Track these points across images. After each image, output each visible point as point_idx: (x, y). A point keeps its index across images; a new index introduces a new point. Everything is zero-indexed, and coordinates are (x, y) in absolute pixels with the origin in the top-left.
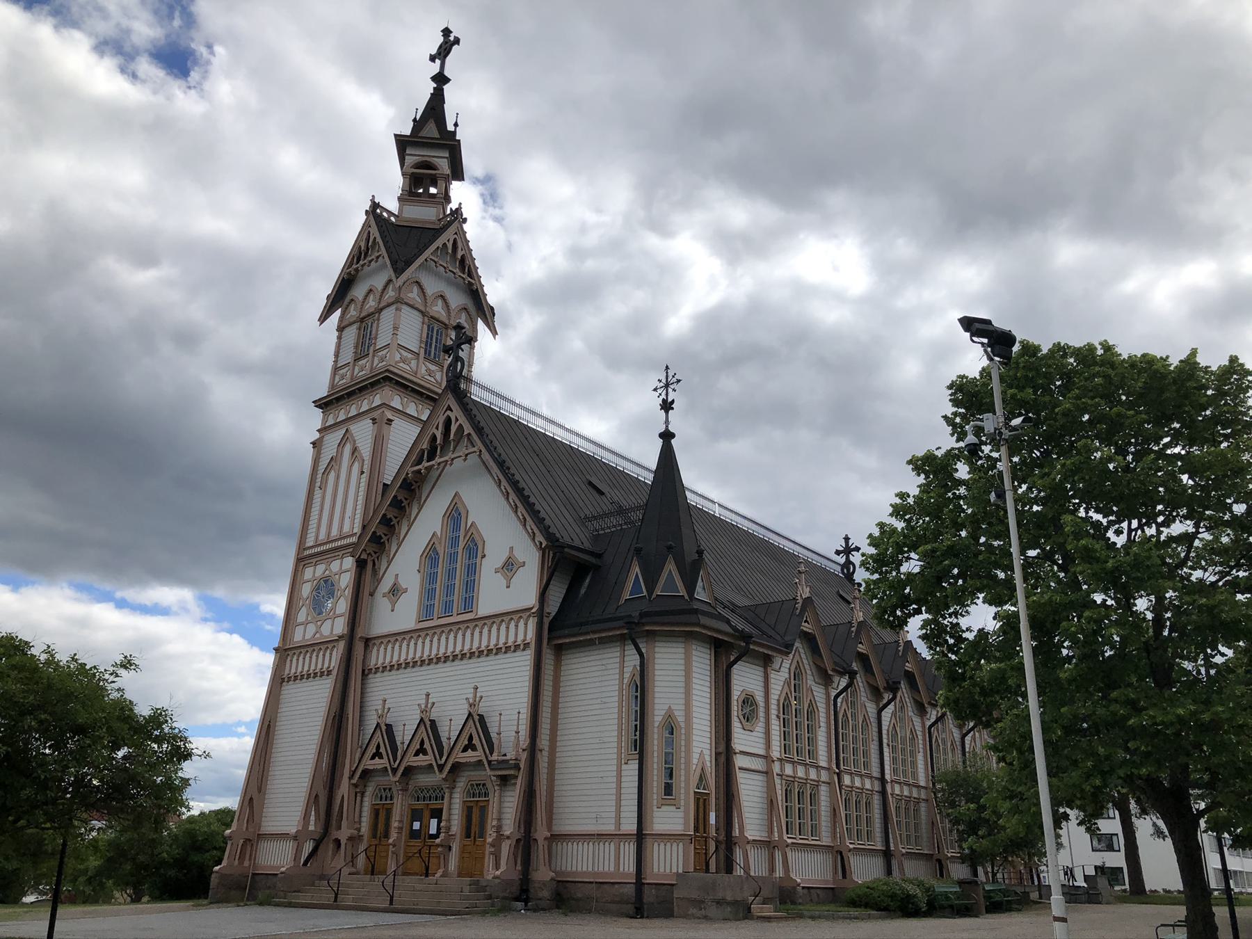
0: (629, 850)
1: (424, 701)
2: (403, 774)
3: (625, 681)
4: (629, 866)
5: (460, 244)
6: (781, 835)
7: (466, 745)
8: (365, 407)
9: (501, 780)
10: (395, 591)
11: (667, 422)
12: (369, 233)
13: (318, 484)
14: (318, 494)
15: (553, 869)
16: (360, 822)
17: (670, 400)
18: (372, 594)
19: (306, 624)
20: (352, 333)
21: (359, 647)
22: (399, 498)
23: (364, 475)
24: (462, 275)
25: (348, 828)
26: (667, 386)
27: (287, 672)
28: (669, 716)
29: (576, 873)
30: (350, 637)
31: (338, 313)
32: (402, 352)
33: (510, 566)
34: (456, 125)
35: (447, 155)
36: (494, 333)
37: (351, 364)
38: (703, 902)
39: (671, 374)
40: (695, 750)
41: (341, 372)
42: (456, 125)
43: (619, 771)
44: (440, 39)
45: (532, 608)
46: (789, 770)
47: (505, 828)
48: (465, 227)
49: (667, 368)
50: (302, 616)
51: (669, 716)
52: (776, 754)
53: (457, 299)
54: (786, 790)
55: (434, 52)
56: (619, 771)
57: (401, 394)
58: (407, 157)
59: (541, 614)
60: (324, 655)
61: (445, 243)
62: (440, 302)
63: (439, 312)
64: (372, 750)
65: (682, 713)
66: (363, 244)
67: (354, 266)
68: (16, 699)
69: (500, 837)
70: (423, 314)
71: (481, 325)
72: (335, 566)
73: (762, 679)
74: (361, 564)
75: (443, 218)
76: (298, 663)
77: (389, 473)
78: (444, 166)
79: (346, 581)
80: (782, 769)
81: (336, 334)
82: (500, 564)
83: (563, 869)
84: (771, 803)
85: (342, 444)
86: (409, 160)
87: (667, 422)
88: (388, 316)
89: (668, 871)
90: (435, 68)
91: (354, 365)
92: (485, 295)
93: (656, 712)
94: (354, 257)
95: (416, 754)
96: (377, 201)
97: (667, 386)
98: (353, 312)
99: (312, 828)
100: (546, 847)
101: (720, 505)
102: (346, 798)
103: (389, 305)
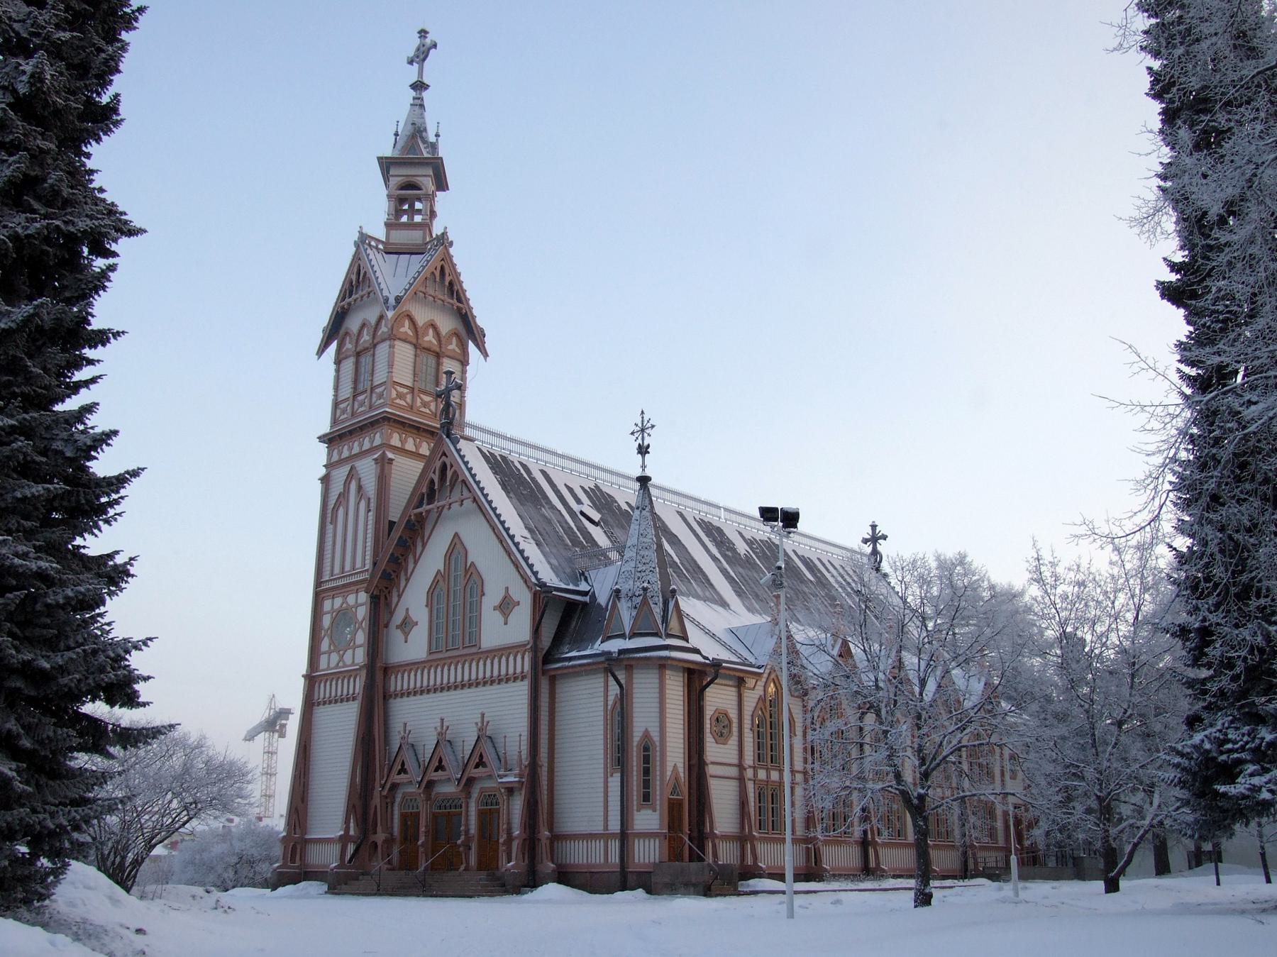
0: (615, 846)
1: (439, 724)
3: (609, 707)
4: (614, 858)
5: (447, 271)
6: (750, 830)
7: (477, 763)
8: (367, 446)
9: (508, 791)
10: (407, 625)
11: (644, 467)
12: (359, 266)
13: (329, 519)
14: (330, 528)
15: (556, 861)
16: (392, 828)
17: (646, 444)
18: (387, 626)
19: (329, 652)
20: (349, 365)
21: (379, 676)
23: (370, 514)
24: (451, 301)
25: (383, 832)
26: (643, 430)
27: (316, 697)
28: (646, 735)
29: (578, 866)
31: (334, 346)
32: (398, 388)
33: (506, 606)
34: (437, 135)
35: (432, 174)
36: (485, 355)
38: (674, 885)
39: (646, 419)
40: (668, 764)
41: (342, 406)
42: (437, 135)
43: (606, 782)
45: (525, 645)
46: (762, 774)
47: (514, 830)
48: (452, 251)
49: (643, 412)
50: (325, 645)
51: (646, 735)
52: (749, 759)
53: (447, 324)
54: (759, 794)
55: (411, 54)
56: (606, 782)
58: (390, 179)
59: (535, 649)
62: (431, 331)
63: (430, 341)
64: (398, 767)
65: (657, 734)
66: (354, 277)
67: (347, 300)
68: (54, 720)
69: (468, 839)
70: (416, 346)
71: (472, 347)
72: (351, 599)
73: (735, 698)
75: (430, 242)
77: (395, 514)
78: (429, 184)
79: (362, 613)
80: (755, 774)
81: (333, 367)
82: (497, 603)
83: (568, 862)
84: (743, 803)
85: (347, 483)
86: (394, 181)
87: (644, 467)
88: (383, 350)
89: (647, 861)
90: (412, 74)
91: (354, 400)
92: (474, 317)
93: (635, 734)
94: (345, 292)
95: (436, 770)
96: (364, 231)
97: (643, 430)
98: (349, 346)
99: (352, 832)
100: (548, 845)
101: (726, 509)
103: (383, 341)
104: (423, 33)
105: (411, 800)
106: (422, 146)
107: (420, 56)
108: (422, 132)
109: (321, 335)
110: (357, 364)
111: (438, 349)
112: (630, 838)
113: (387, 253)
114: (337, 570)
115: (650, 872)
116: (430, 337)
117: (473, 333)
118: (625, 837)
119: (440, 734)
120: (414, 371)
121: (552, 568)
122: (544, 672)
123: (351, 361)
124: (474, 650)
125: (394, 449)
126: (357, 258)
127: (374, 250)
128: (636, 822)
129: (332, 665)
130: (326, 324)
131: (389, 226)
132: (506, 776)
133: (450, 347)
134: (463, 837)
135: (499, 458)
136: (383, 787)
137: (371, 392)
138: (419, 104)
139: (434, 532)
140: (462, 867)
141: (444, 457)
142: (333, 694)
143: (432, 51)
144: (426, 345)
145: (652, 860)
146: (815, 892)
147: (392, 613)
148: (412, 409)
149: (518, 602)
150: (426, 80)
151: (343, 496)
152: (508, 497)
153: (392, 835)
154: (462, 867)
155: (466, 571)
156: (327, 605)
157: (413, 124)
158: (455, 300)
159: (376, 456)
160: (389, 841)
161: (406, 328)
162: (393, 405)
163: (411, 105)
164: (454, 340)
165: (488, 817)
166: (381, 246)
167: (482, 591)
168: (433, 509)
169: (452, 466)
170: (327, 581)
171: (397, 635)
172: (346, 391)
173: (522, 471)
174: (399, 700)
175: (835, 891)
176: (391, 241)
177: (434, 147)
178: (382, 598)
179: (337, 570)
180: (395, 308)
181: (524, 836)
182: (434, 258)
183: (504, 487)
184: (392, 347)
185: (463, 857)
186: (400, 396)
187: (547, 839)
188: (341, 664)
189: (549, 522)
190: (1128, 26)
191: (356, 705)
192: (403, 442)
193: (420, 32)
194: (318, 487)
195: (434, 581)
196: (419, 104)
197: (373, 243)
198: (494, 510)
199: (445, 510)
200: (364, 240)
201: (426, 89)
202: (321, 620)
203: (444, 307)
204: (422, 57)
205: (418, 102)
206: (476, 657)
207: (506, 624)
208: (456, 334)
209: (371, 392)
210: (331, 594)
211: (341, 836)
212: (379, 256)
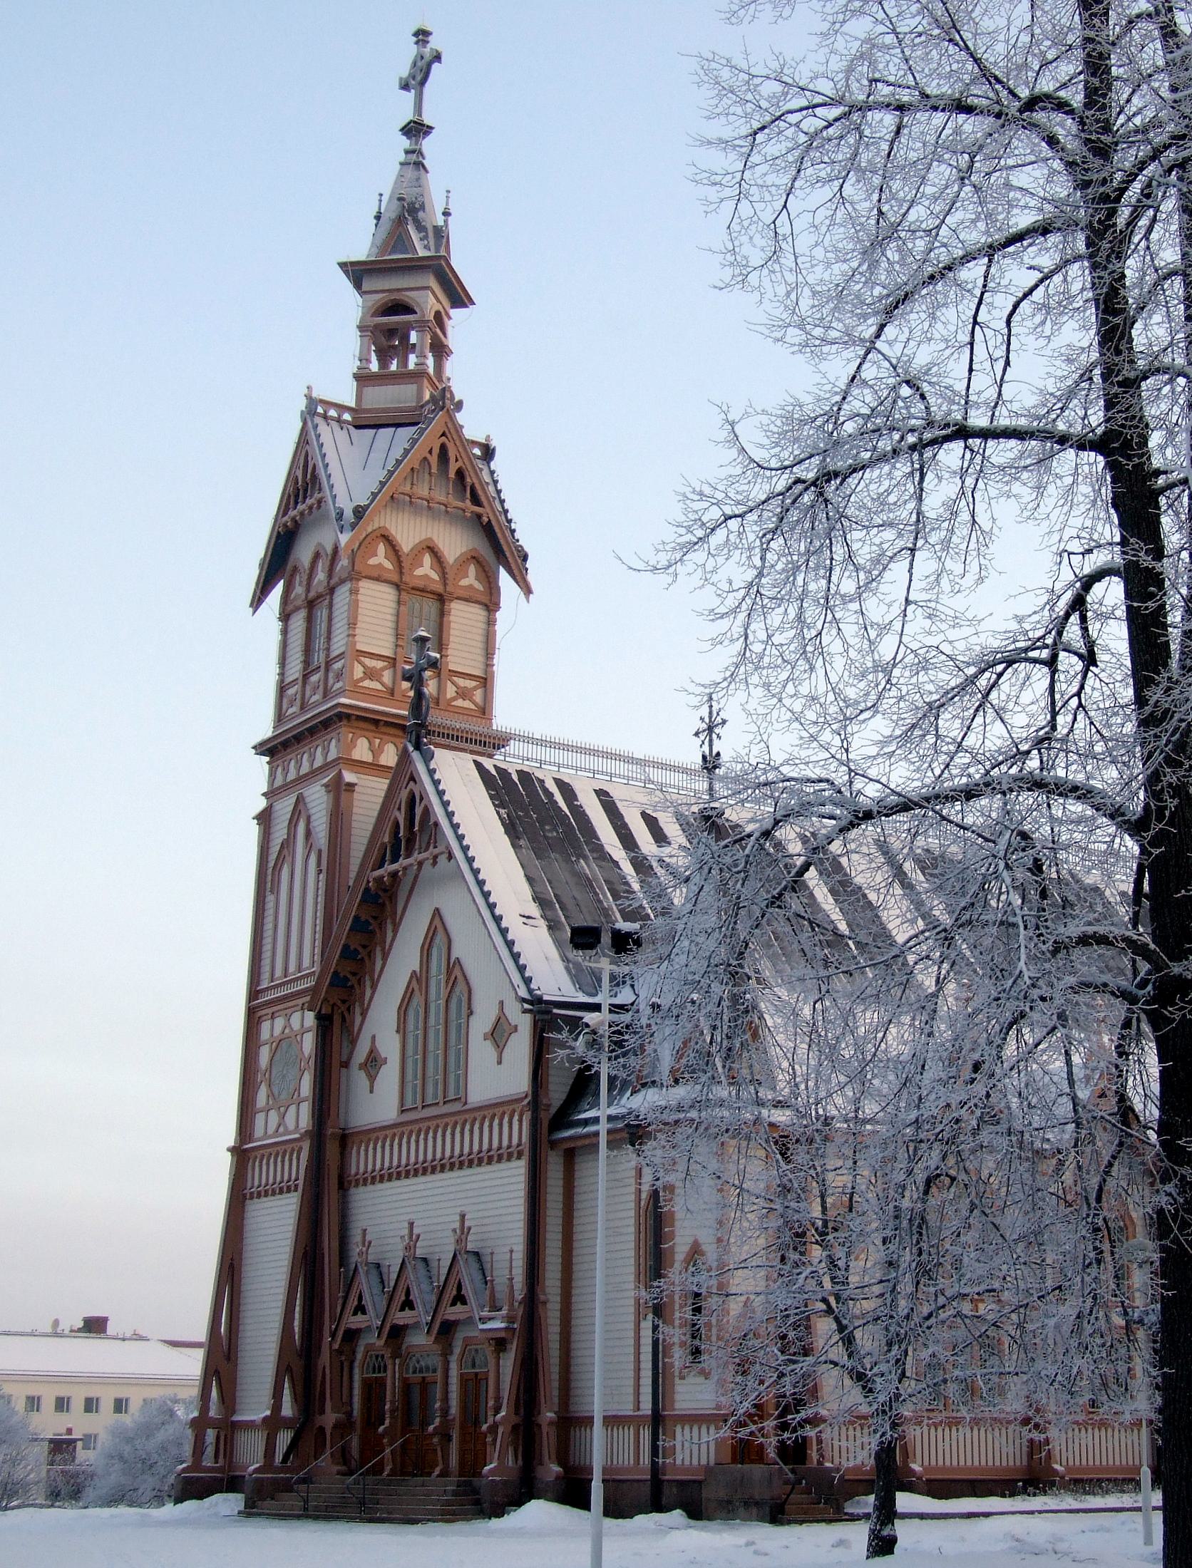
2: (389, 1336)
5: (452, 454)
10: (373, 1063)
14: (270, 899)
16: (351, 1404)
18: (346, 1064)
20: (298, 622)
21: (332, 1150)
22: (363, 919)
24: (460, 504)
30: (318, 1134)
31: (278, 590)
34: (446, 214)
36: (528, 590)
37: (300, 682)
42: (446, 214)
44: (408, 51)
45: (522, 1099)
48: (461, 417)
50: (262, 1098)
55: (405, 73)
57: (367, 734)
60: (491, 1127)
61: (425, 459)
62: (427, 559)
66: (300, 474)
67: (292, 513)
70: (397, 586)
71: (504, 578)
74: (325, 1024)
76: (392, 1149)
79: (309, 1043)
81: (277, 626)
82: (488, 1027)
85: (293, 823)
88: (342, 595)
89: (695, 1462)
90: (404, 108)
96: (314, 395)
102: (328, 1371)
103: (342, 582)
104: (422, 35)
105: (377, 1357)
106: (414, 236)
107: (417, 79)
108: (418, 210)
109: (257, 572)
110: (310, 620)
111: (439, 588)
112: (669, 1423)
113: (358, 427)
114: (278, 973)
115: (700, 1482)
116: (426, 569)
117: (505, 555)
118: (658, 1421)
119: (407, 1248)
120: (397, 629)
121: (567, 969)
122: (553, 1144)
123: (302, 614)
124: (456, 1107)
125: (359, 766)
126: (305, 445)
127: (334, 424)
128: (677, 1397)
129: (271, 1131)
130: (262, 555)
131: (363, 379)
132: (490, 1319)
133: (464, 582)
134: (437, 1421)
135: (515, 777)
136: (333, 1335)
137: (327, 670)
138: (415, 162)
139: (411, 903)
140: (437, 1471)
141: (412, 783)
142: (476, 1148)
143: (435, 66)
144: (420, 584)
145: (704, 1462)
146: (987, 1515)
147: (353, 1042)
148: (392, 694)
149: (516, 1027)
150: (427, 121)
151: (288, 844)
152: (514, 845)
153: (349, 1414)
154: (437, 1471)
155: (449, 971)
156: (265, 1030)
157: (400, 199)
158: (468, 502)
159: (325, 781)
160: (344, 1427)
161: (380, 558)
162: (357, 691)
163: (401, 164)
164: (472, 570)
165: (473, 1385)
166: (347, 417)
167: (469, 1007)
168: (411, 865)
169: (421, 799)
170: (267, 989)
171: (360, 1078)
172: (295, 670)
173: (558, 797)
174: (361, 1189)
175: (1032, 1513)
176: (364, 407)
177: (440, 235)
178: (337, 1019)
179: (278, 973)
180: (353, 526)
181: (515, 1420)
182: (430, 436)
183: (511, 829)
184: (354, 592)
185: (439, 1453)
186: (370, 674)
187: (551, 1423)
188: (281, 1129)
189: (588, 883)
190: (737, 249)
191: (295, 1200)
192: (376, 752)
193: (416, 34)
194: (254, 830)
195: (406, 992)
196: (415, 162)
197: (333, 413)
198: (476, 872)
199: (427, 866)
200: (314, 410)
201: (427, 133)
202: (257, 1054)
203: (449, 515)
204: (419, 78)
205: (414, 157)
206: (460, 1118)
207: (500, 1062)
208: (475, 559)
209: (327, 670)
210: (270, 1011)
211: (265, 1419)
212: (342, 436)
